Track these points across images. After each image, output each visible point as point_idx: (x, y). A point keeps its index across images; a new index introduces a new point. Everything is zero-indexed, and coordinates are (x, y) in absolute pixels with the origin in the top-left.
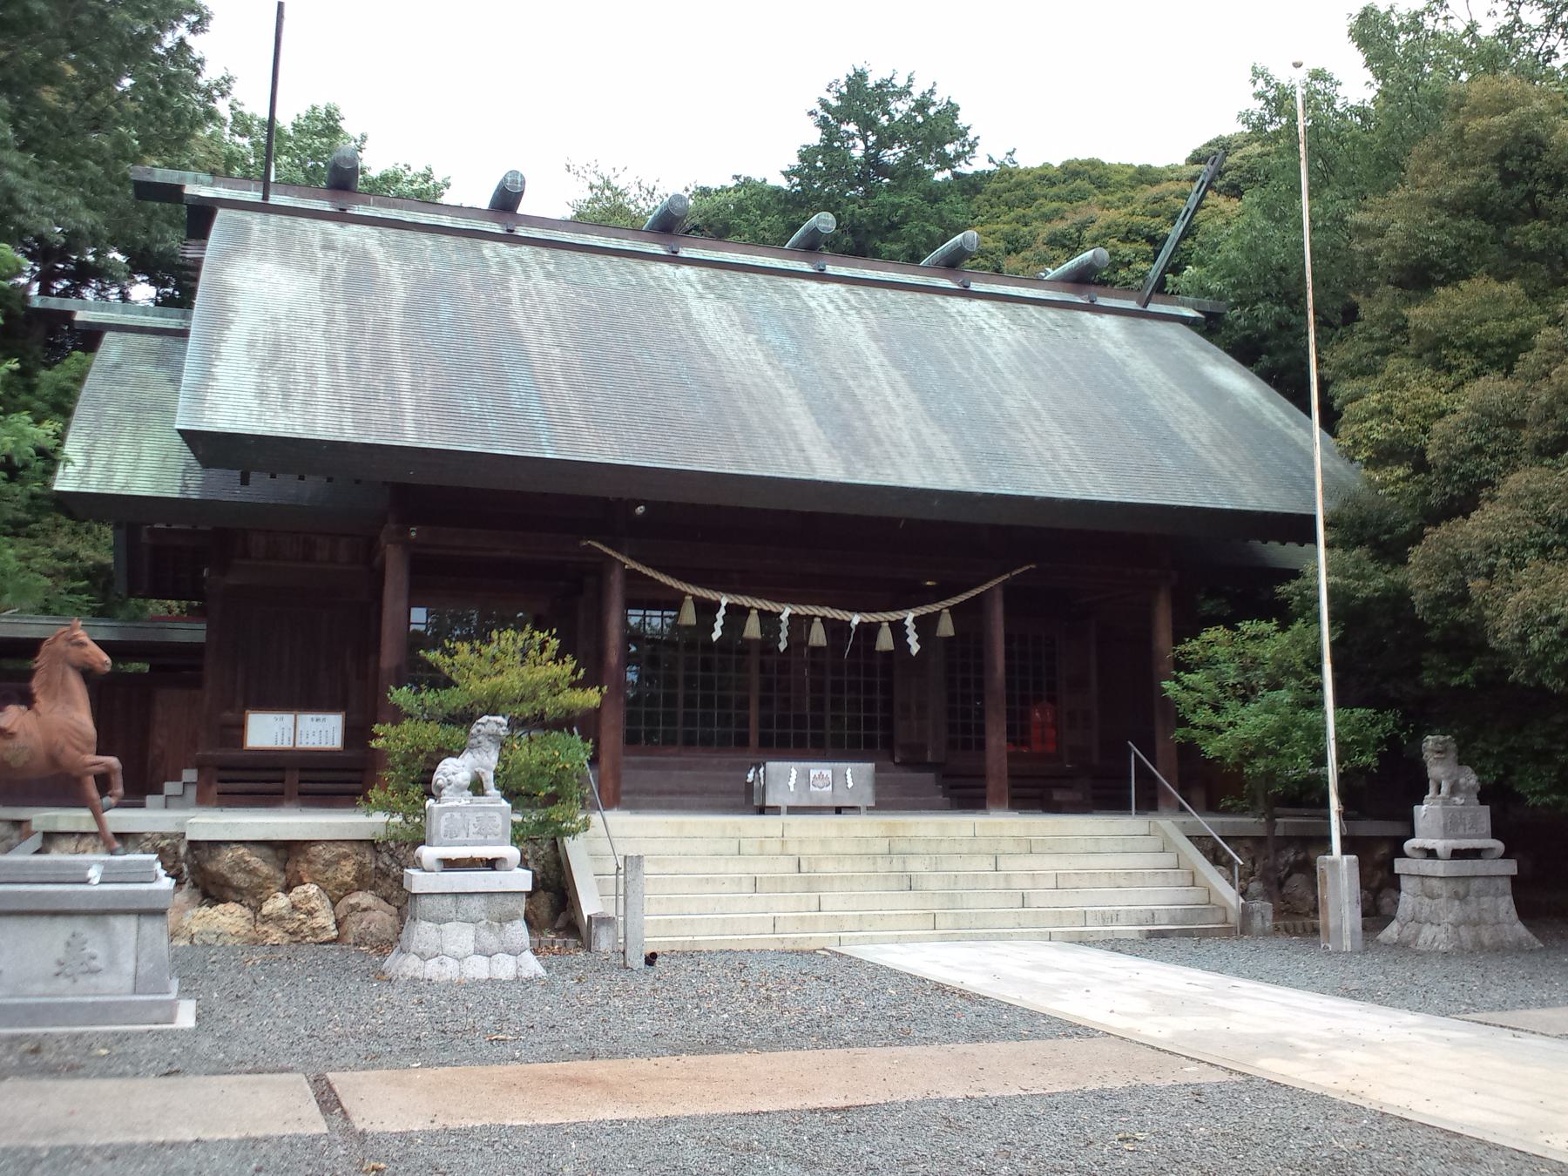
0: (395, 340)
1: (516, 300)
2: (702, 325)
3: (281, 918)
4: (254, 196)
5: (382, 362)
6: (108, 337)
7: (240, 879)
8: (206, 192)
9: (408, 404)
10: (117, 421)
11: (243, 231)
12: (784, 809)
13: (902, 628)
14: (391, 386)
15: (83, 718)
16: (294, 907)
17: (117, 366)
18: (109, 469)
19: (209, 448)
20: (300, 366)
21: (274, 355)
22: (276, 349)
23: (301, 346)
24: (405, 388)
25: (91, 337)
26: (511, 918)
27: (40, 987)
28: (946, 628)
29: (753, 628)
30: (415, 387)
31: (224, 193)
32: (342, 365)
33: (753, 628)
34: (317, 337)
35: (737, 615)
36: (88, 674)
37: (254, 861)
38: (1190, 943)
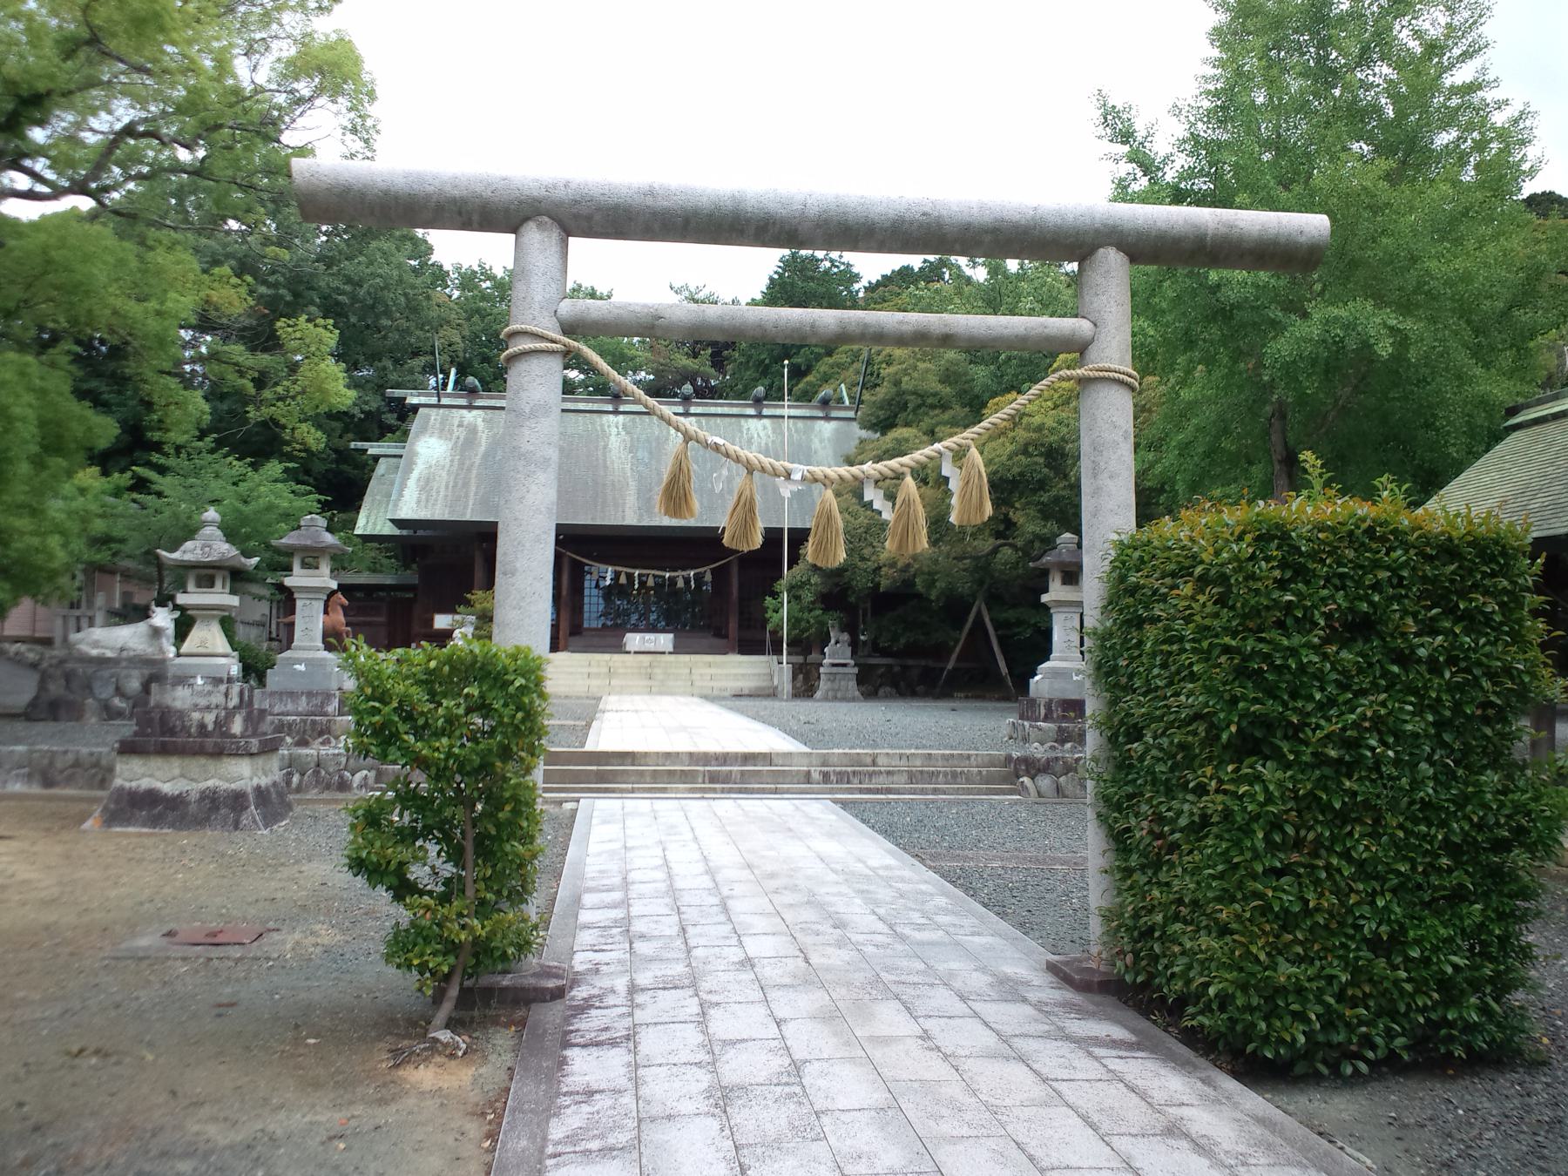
4: (434, 400)
5: (466, 484)
10: (380, 502)
11: (428, 417)
13: (683, 577)
14: (467, 496)
15: (342, 618)
18: (375, 524)
19: (399, 523)
21: (426, 484)
25: (415, 409)
29: (623, 580)
31: (423, 400)
33: (623, 580)
34: (444, 474)
35: (617, 575)
36: (343, 607)
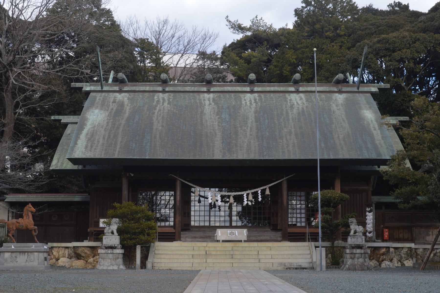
0: (121, 129)
1: (156, 113)
2: (205, 114)
3: (91, 263)
4: (99, 88)
6: (69, 126)
7: (83, 254)
8: (88, 89)
9: (118, 147)
12: (221, 241)
16: (94, 261)
17: (69, 134)
19: (74, 161)
20: (97, 139)
22: (92, 135)
23: (98, 133)
24: (119, 142)
26: (118, 258)
27: (24, 264)
28: (268, 192)
30: (121, 142)
31: (93, 88)
32: (106, 138)
37: (86, 251)
38: (295, 271)
